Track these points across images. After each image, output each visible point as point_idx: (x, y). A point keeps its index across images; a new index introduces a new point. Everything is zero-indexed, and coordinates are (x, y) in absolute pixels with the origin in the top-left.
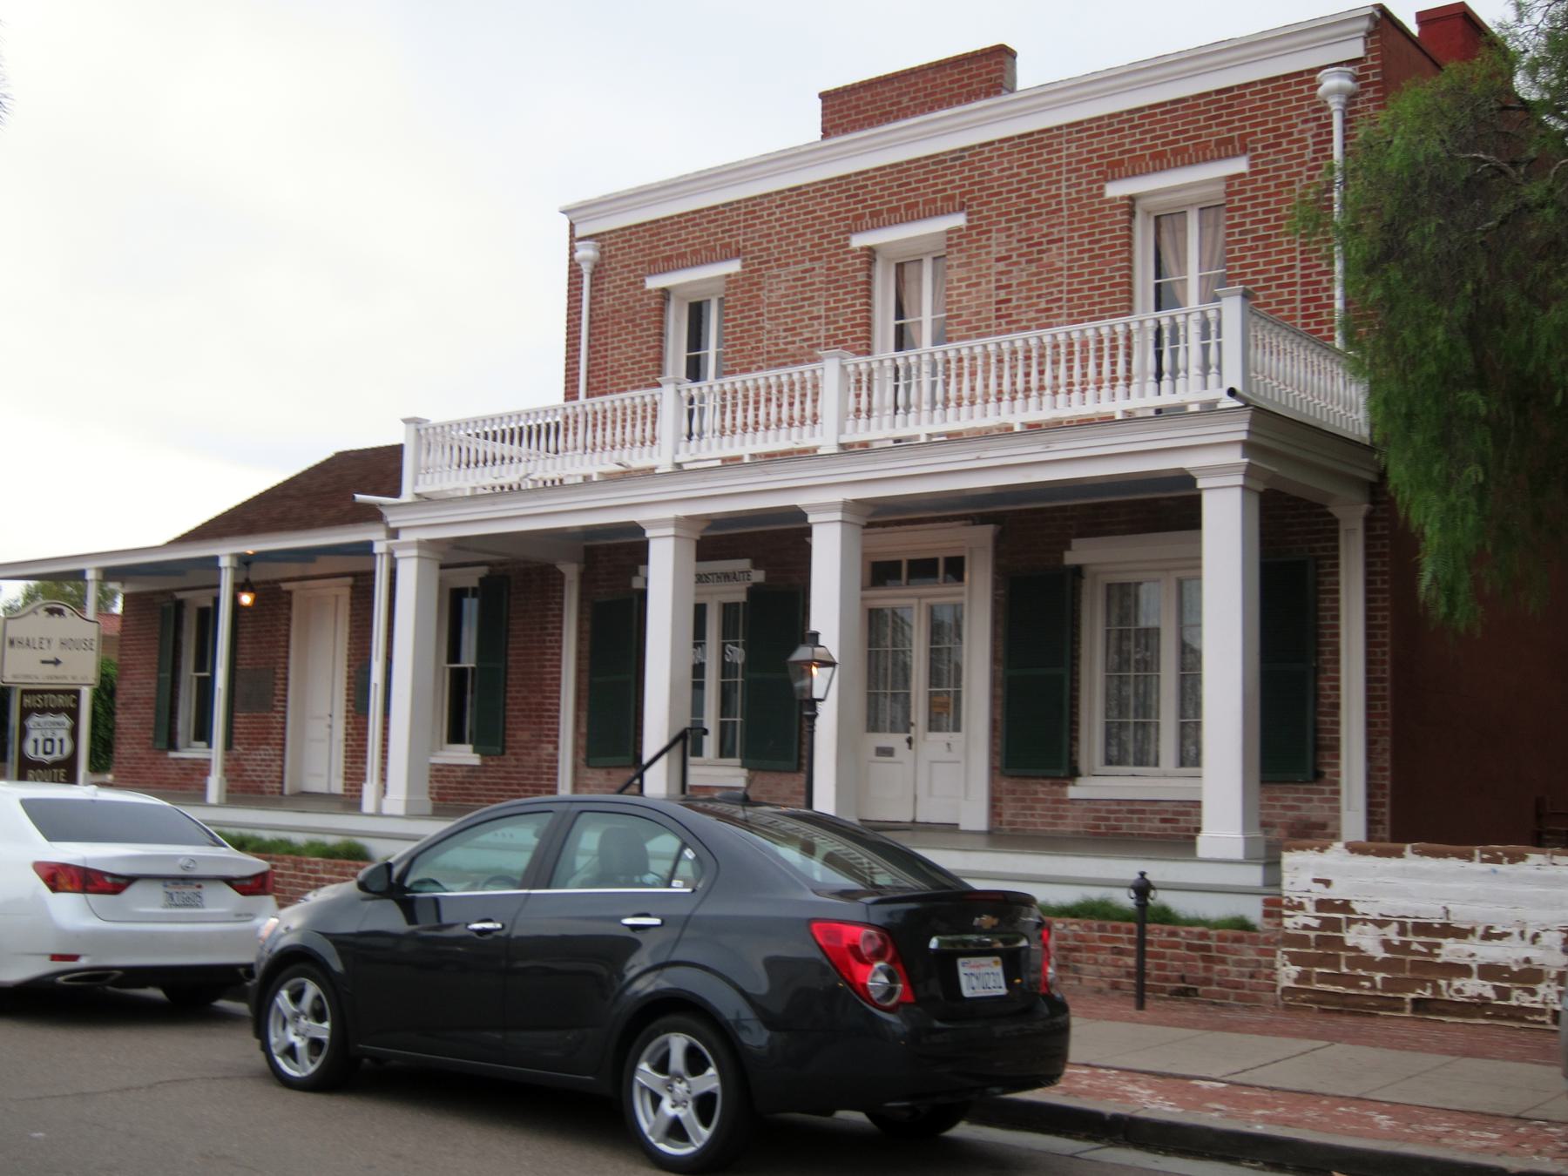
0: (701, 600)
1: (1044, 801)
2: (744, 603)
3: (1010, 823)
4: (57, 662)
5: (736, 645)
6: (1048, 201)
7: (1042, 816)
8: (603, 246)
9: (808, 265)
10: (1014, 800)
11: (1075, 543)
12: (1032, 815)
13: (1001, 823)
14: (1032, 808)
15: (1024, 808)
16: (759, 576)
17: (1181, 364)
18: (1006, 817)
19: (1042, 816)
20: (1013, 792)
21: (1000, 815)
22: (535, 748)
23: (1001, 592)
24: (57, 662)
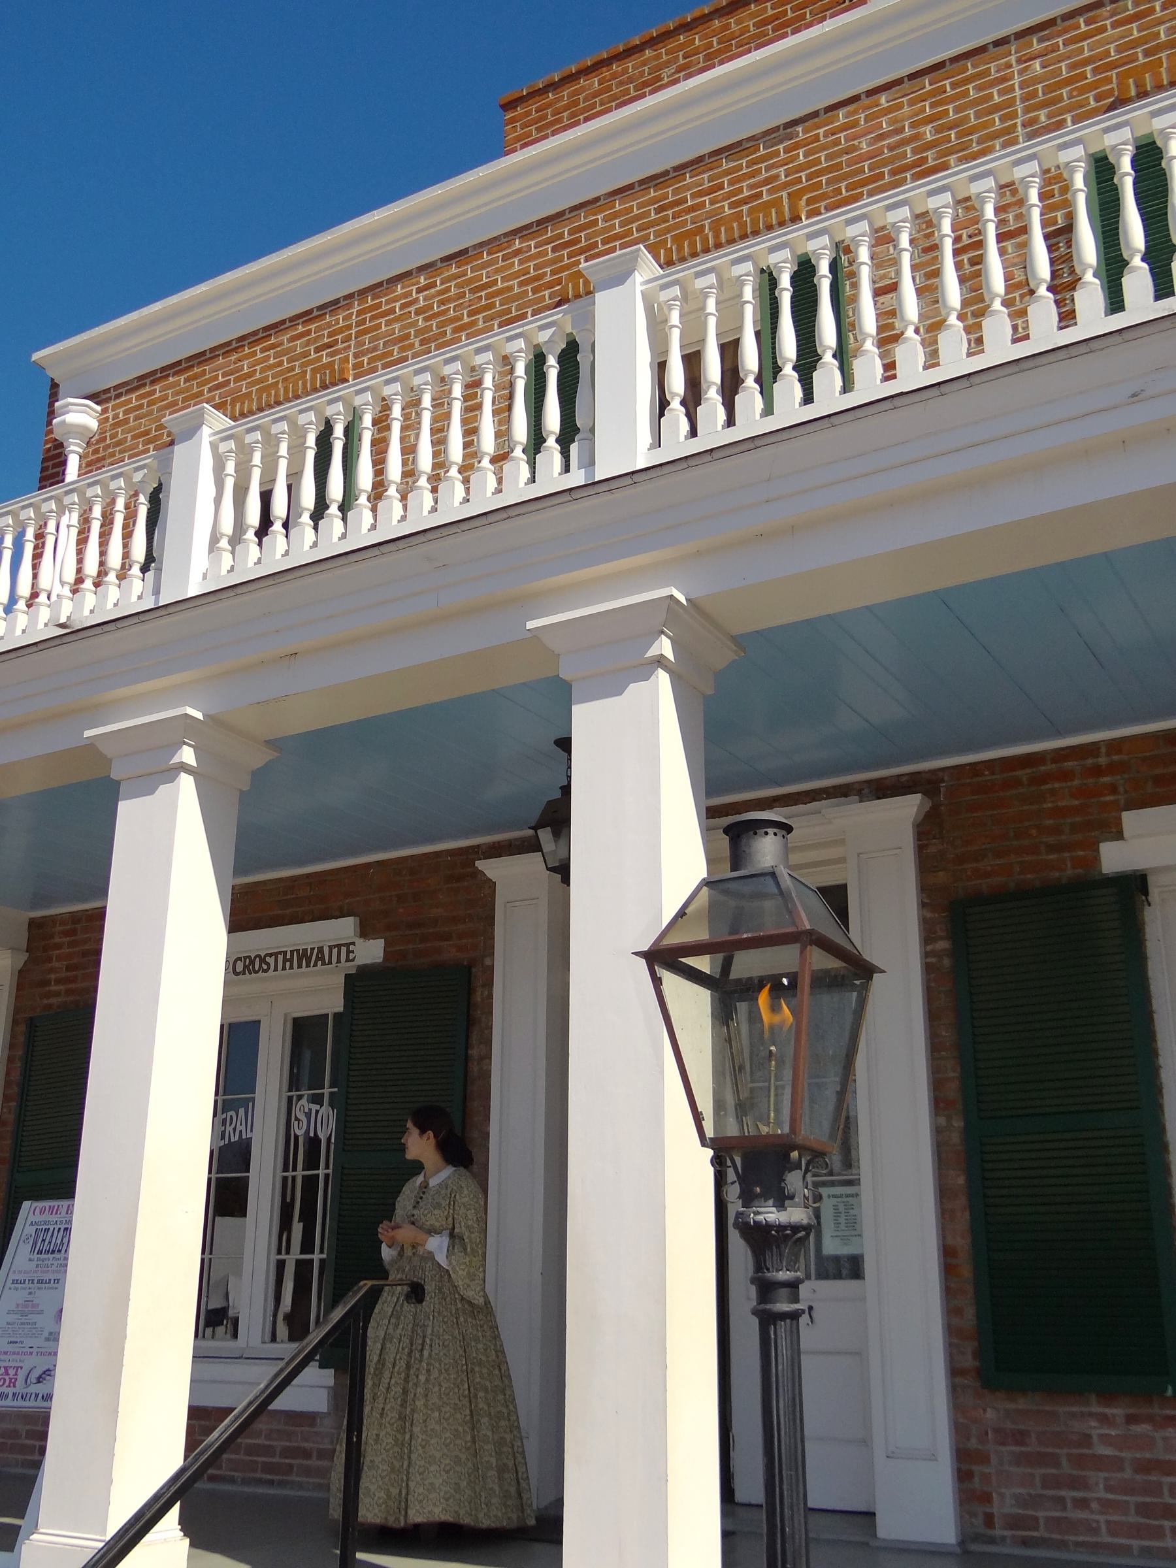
0: (245, 1015)
1: (1116, 1464)
2: (337, 1015)
3: (1014, 1523)
5: (317, 1100)
6: (774, 172)
7: (1106, 1505)
8: (104, 411)
10: (1020, 1460)
11: (1130, 819)
12: (1083, 1504)
13: (989, 1520)
14: (1076, 1483)
15: (1050, 1482)
16: (371, 952)
17: (791, 1423)
18: (1004, 1504)
19: (1106, 1505)
20: (1020, 1437)
21: (986, 1498)
23: (942, 945)
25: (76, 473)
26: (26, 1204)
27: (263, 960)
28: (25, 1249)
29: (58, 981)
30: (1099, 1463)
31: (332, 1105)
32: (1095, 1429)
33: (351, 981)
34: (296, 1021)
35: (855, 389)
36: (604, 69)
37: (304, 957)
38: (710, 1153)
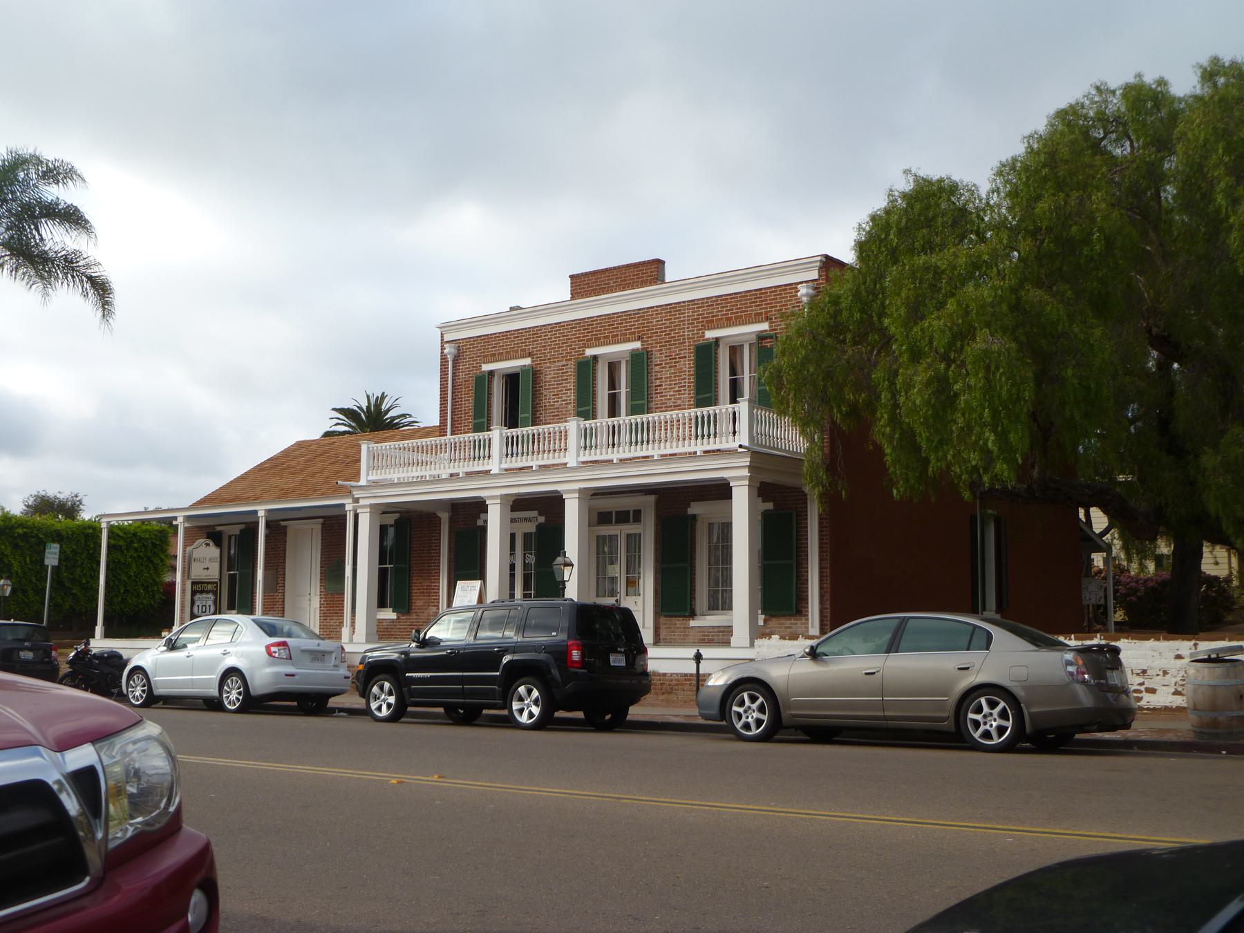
4: (208, 569)
9: (564, 363)
10: (666, 628)
16: (542, 519)
22: (426, 609)
24: (208, 569)
25: (745, 346)
26: (458, 582)
27: (515, 520)
28: (460, 590)
29: (462, 521)
30: (678, 628)
31: (535, 555)
32: (678, 622)
33: (537, 527)
34: (525, 534)
35: (1132, 727)
36: (532, 559)
37: (526, 520)
38: (635, 667)
